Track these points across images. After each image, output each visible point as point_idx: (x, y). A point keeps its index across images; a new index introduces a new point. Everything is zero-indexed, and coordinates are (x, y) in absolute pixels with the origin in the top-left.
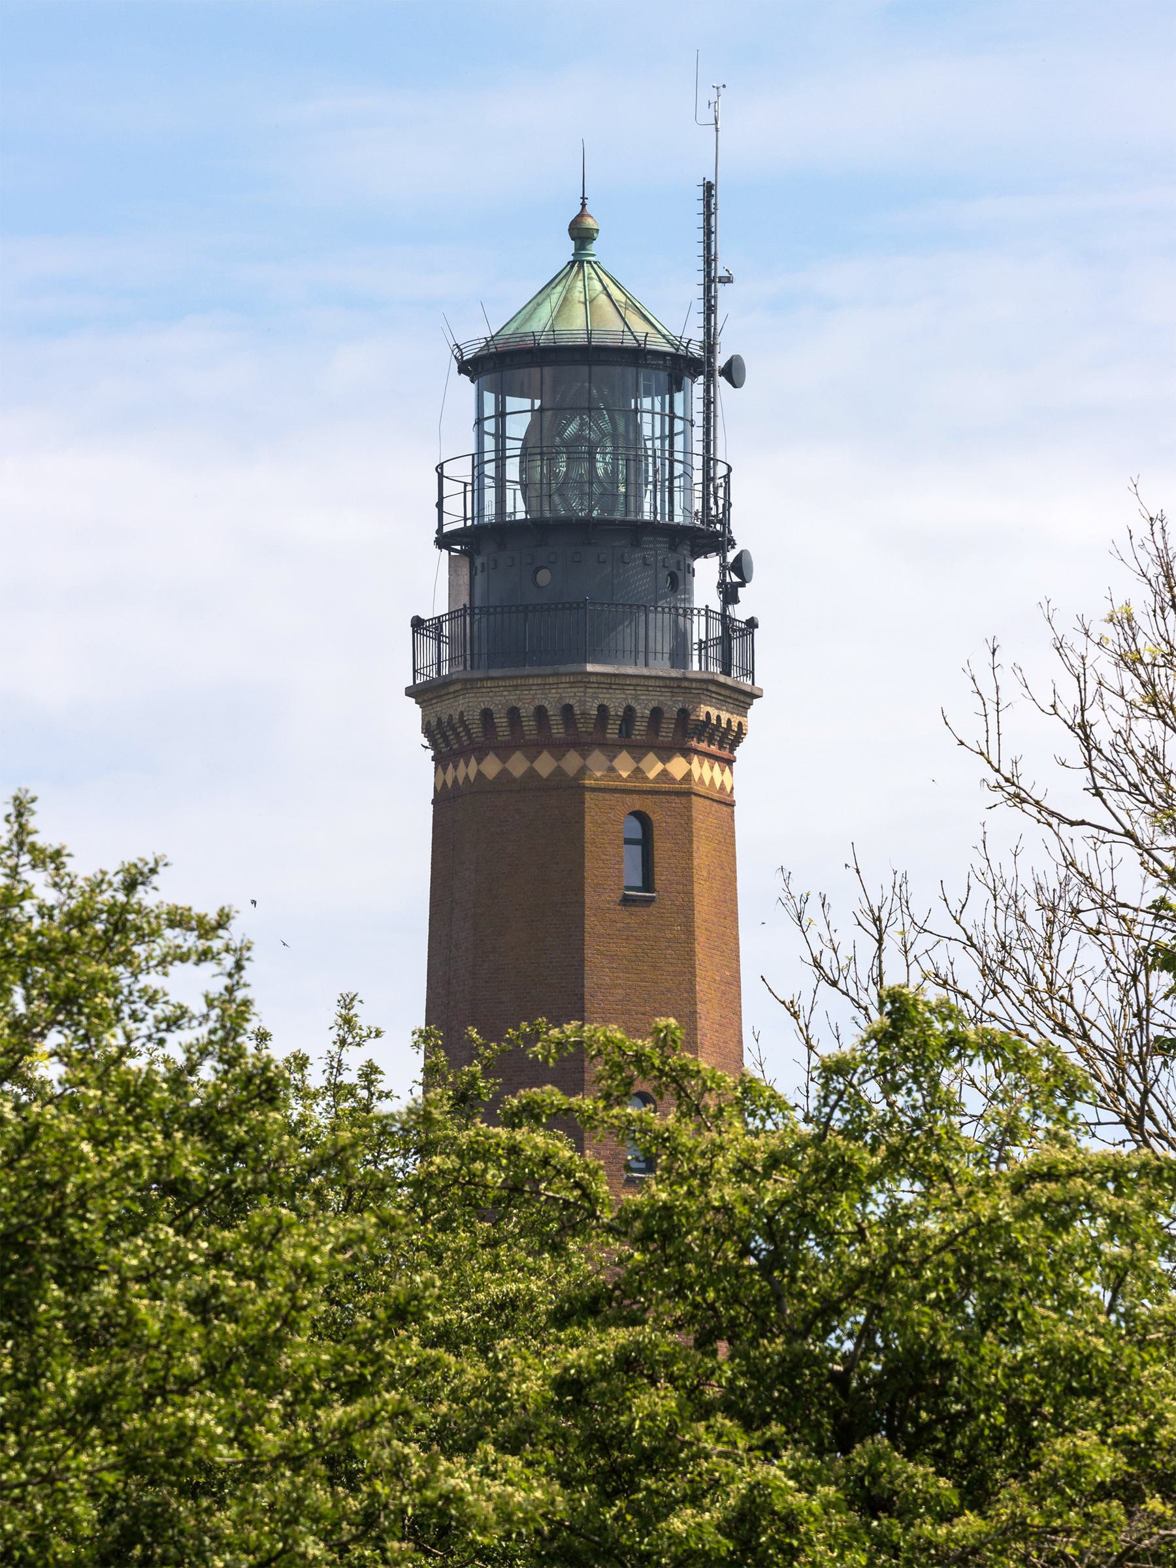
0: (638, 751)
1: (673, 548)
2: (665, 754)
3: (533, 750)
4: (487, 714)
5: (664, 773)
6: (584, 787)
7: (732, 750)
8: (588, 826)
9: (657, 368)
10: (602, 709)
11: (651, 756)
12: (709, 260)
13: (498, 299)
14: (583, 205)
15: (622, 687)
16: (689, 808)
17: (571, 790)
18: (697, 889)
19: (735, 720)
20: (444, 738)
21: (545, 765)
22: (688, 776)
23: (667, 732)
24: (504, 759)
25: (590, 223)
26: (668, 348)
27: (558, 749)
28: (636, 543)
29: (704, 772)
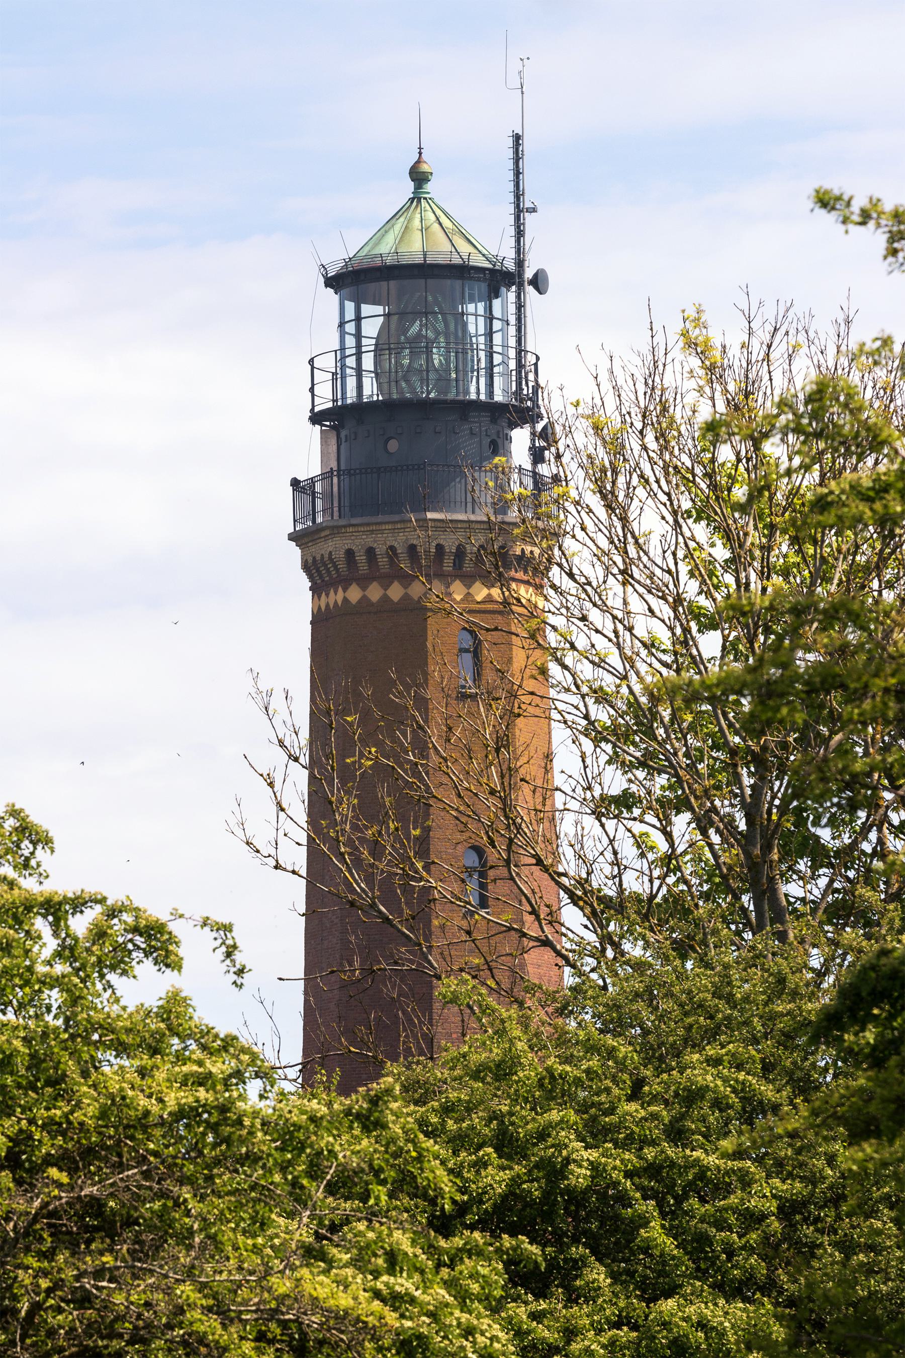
1: (494, 421)
4: (350, 553)
6: (426, 609)
9: (479, 280)
10: (440, 547)
12: (518, 195)
14: (420, 153)
15: (455, 530)
17: (415, 613)
20: (321, 575)
21: (396, 592)
24: (364, 589)
25: (425, 168)
26: (487, 265)
28: (464, 418)
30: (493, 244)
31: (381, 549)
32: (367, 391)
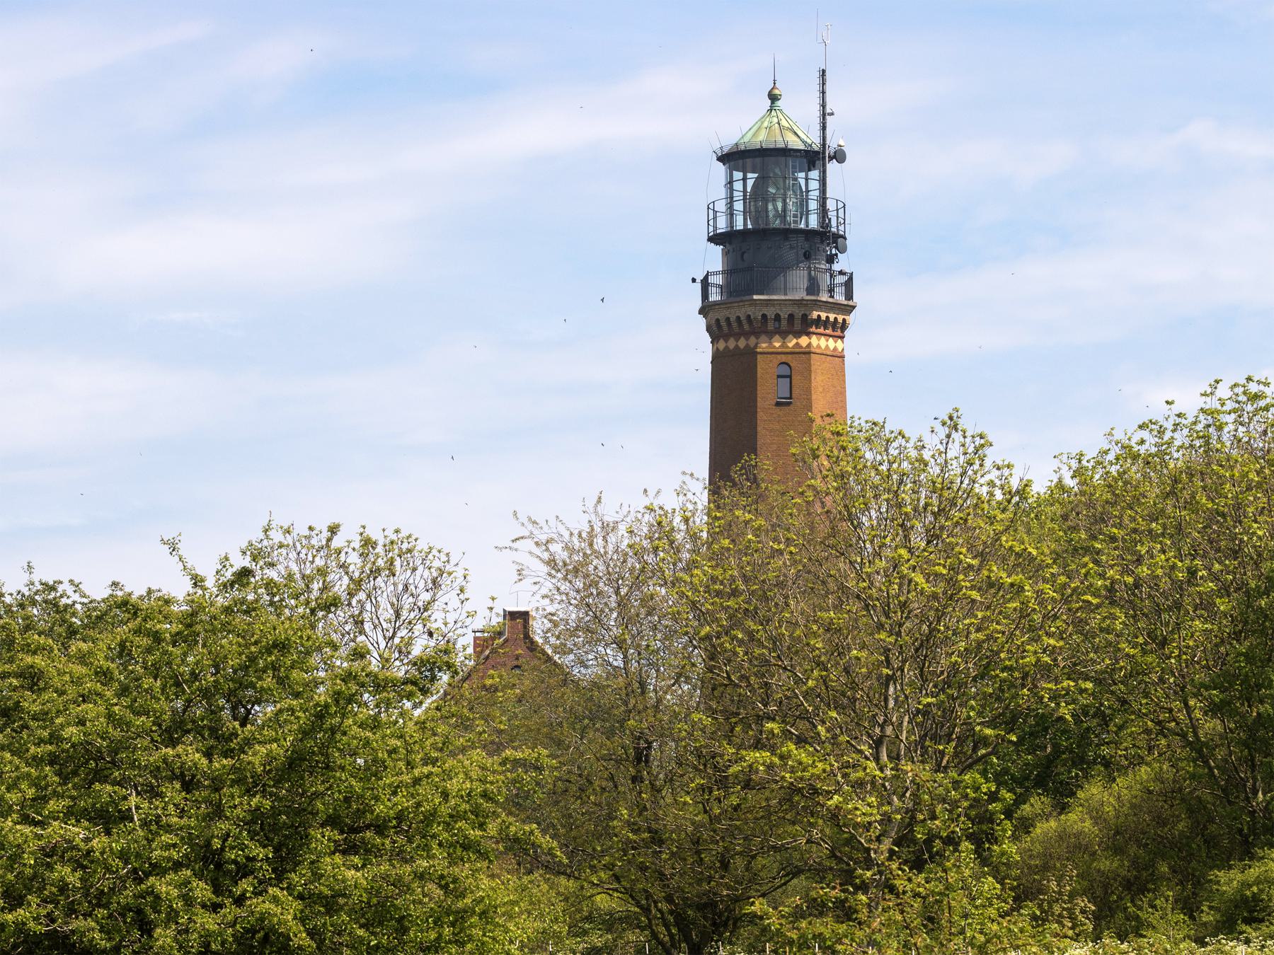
0: (784, 335)
1: (807, 239)
2: (798, 334)
3: (737, 337)
7: (843, 331)
8: (759, 370)
10: (764, 316)
12: (823, 106)
13: (743, 124)
15: (773, 305)
17: (751, 354)
18: (814, 397)
19: (840, 318)
20: (715, 332)
21: (742, 343)
22: (809, 345)
23: (798, 326)
24: (726, 341)
25: (776, 92)
26: (802, 147)
27: (747, 335)
28: (787, 239)
29: (820, 342)
30: (805, 134)
31: (733, 319)
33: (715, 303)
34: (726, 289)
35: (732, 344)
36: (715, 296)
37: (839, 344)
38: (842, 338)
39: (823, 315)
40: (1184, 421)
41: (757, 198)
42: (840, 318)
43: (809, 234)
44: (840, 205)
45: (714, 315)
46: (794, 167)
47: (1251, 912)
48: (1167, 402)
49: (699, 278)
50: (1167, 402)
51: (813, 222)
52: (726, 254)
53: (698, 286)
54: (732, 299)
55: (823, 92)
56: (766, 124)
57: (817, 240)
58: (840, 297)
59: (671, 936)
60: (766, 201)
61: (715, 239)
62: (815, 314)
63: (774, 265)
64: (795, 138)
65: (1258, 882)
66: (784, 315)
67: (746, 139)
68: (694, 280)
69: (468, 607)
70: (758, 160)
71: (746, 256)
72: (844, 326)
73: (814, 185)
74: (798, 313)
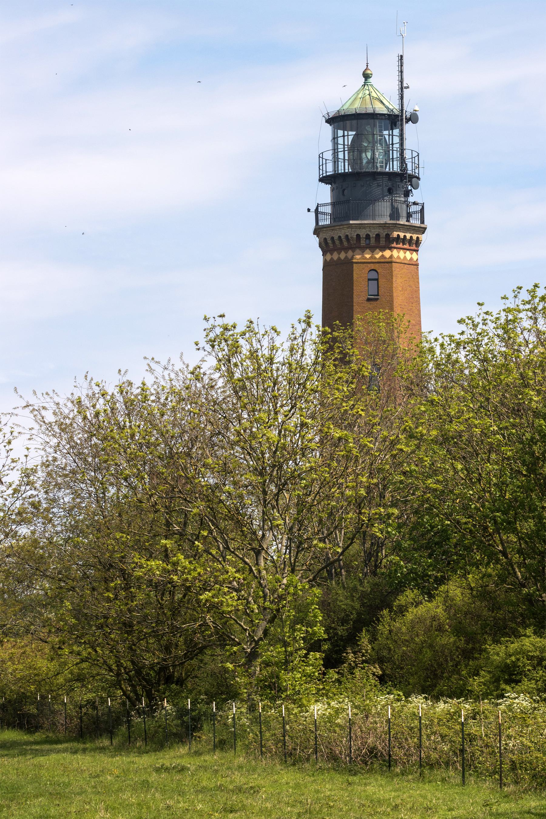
0: (373, 249)
1: (390, 179)
2: (383, 249)
3: (339, 251)
5: (383, 256)
6: (353, 263)
9: (382, 119)
10: (358, 236)
11: (378, 250)
12: (402, 82)
15: (364, 228)
16: (392, 267)
17: (349, 263)
19: (415, 237)
20: (325, 247)
21: (343, 256)
22: (391, 256)
23: (383, 242)
24: (332, 254)
25: (369, 72)
26: (385, 111)
27: (346, 250)
28: (375, 179)
29: (399, 254)
31: (336, 238)
32: (395, 167)
33: (324, 227)
34: (334, 217)
35: (335, 256)
36: (326, 221)
37: (415, 256)
38: (417, 251)
39: (402, 235)
40: (490, 317)
41: (355, 148)
42: (415, 237)
43: (392, 175)
44: (415, 154)
45: (323, 235)
46: (380, 127)
47: (511, 674)
48: (479, 304)
49: (313, 209)
50: (479, 304)
51: (396, 167)
52: (332, 190)
53: (313, 215)
54: (336, 224)
55: (402, 72)
56: (360, 96)
57: (398, 179)
58: (415, 222)
59: (135, 691)
60: (360, 152)
61: (324, 180)
62: (395, 234)
63: (367, 196)
64: (381, 106)
65: (516, 653)
66: (373, 235)
67: (345, 107)
68: (309, 210)
69: (12, 455)
70: (354, 122)
71: (346, 191)
72: (418, 243)
73: (396, 140)
74: (383, 233)
